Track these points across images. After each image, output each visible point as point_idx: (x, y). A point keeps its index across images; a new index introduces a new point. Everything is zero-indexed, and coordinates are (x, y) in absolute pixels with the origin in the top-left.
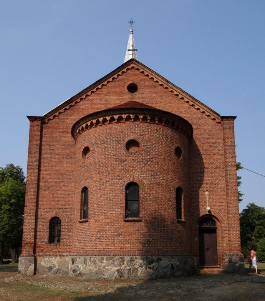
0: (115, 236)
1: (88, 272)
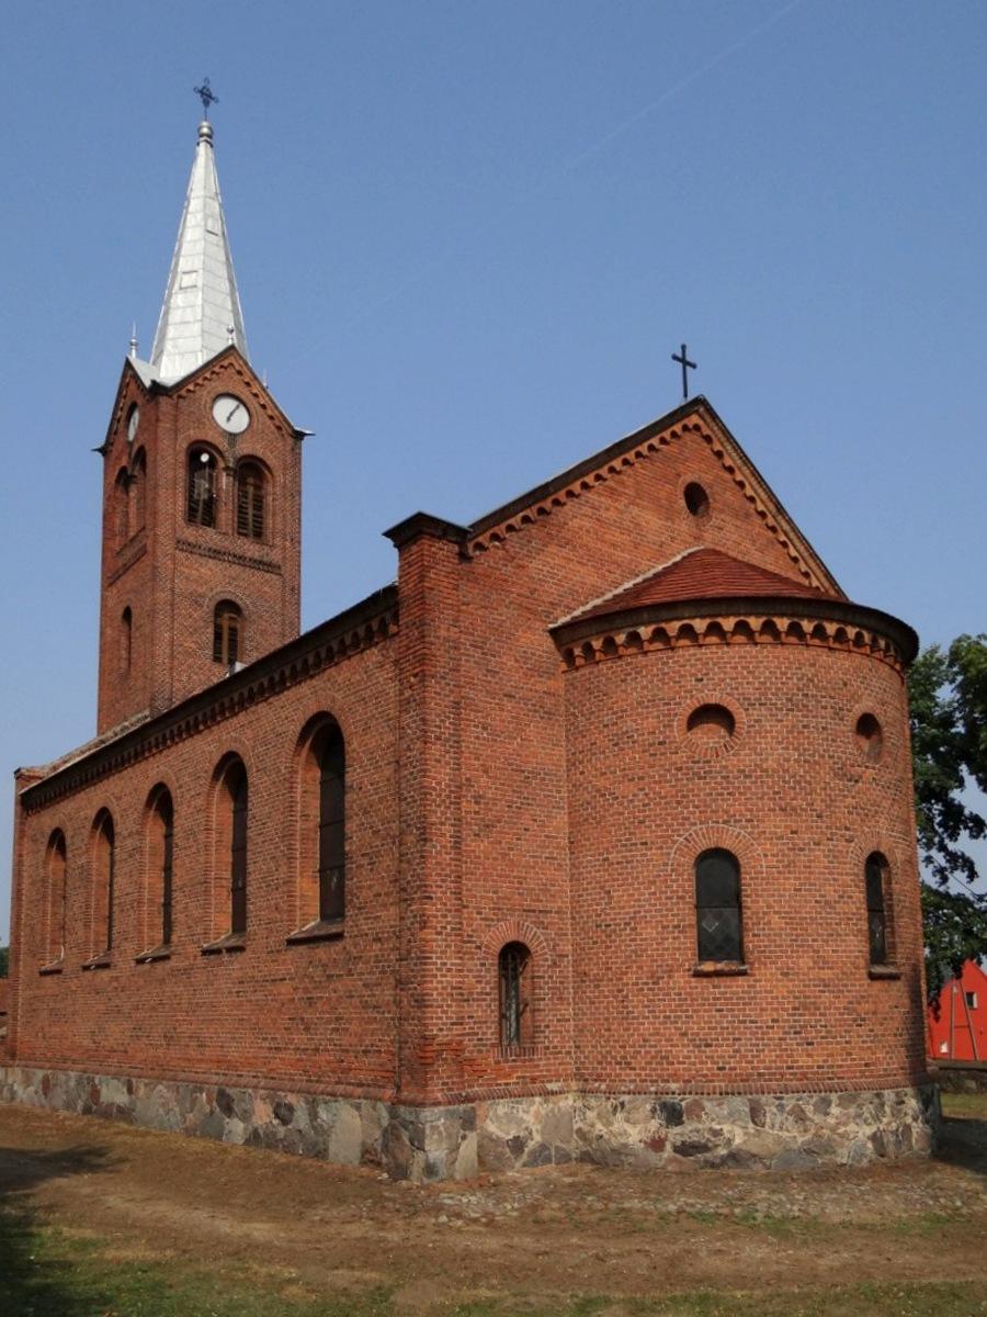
0: (850, 1025)
1: (778, 1149)
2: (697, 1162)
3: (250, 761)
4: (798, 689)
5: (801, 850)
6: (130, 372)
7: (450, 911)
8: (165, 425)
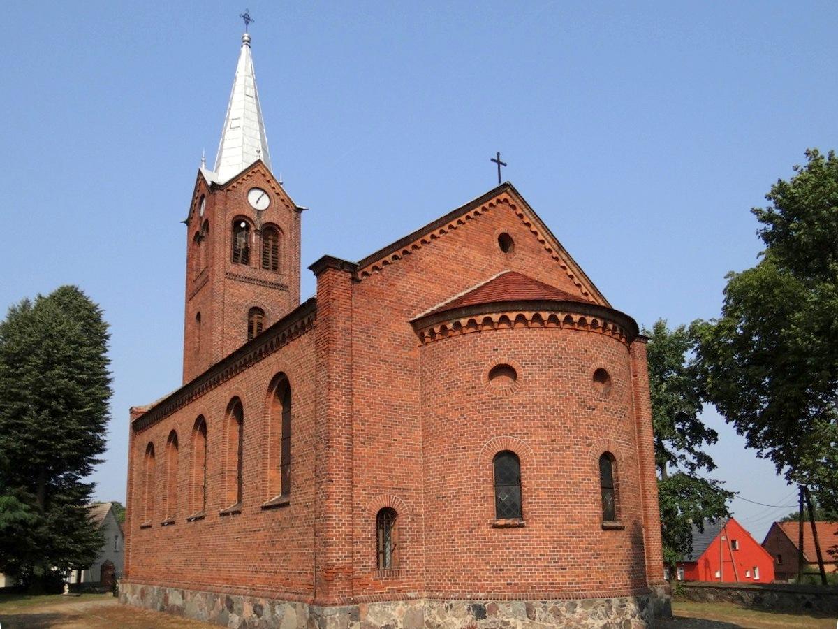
0: (590, 558)
3: (244, 402)
4: (556, 355)
6: (201, 177)
7: (344, 489)
8: (219, 207)
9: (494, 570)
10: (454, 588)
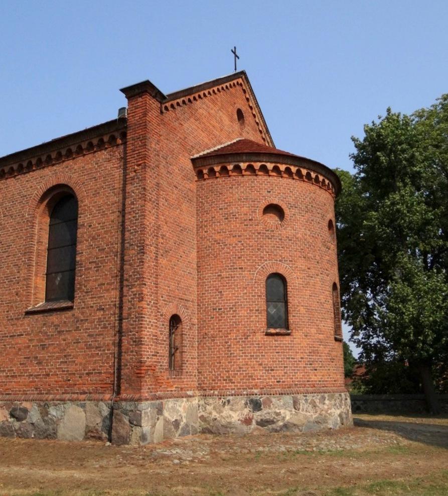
1: (305, 421)
2: (269, 430)
4: (310, 203)
5: (312, 277)
9: (266, 370)
10: (229, 386)
